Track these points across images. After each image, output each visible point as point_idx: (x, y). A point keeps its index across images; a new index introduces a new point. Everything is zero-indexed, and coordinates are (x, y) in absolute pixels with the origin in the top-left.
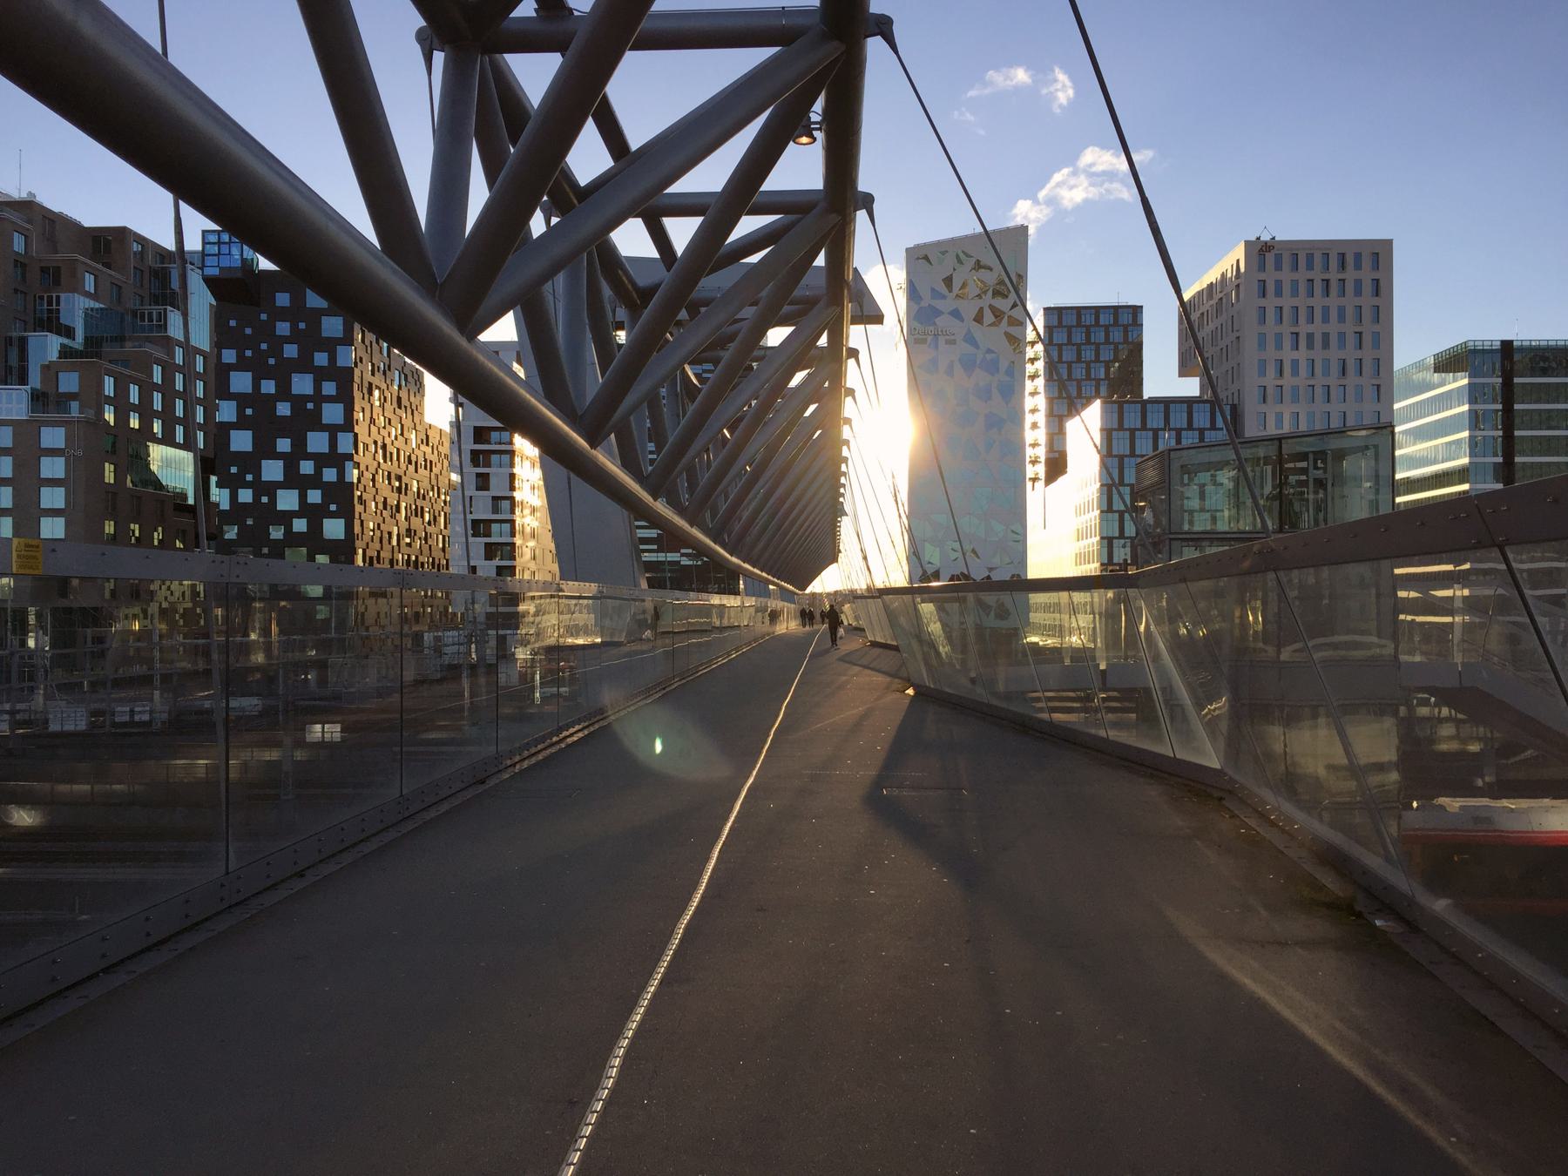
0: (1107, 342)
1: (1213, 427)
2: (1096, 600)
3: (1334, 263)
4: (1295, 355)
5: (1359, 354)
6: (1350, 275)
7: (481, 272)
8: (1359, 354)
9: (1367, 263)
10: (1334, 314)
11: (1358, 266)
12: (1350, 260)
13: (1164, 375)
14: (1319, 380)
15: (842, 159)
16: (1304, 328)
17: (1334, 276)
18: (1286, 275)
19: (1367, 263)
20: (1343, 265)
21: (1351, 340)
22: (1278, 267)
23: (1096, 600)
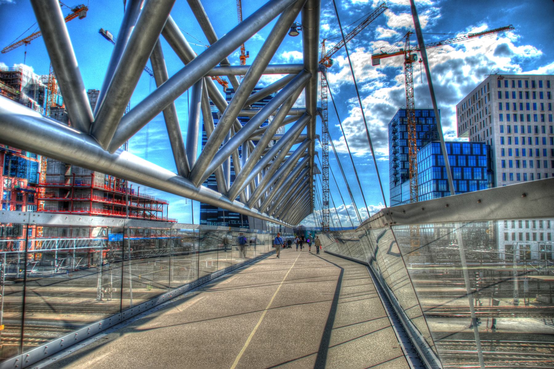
0: (426, 124)
1: (483, 179)
2: (326, 15)
3: (530, 84)
4: (515, 123)
5: (543, 124)
6: (538, 90)
7: (21, 346)
8: (543, 124)
9: (544, 85)
10: (524, 95)
11: (541, 86)
12: (537, 83)
13: (450, 131)
14: (527, 135)
15: (311, 43)
16: (519, 112)
17: (530, 90)
18: (510, 89)
19: (544, 85)
20: (534, 86)
21: (539, 118)
22: (506, 85)
23: (326, 15)
